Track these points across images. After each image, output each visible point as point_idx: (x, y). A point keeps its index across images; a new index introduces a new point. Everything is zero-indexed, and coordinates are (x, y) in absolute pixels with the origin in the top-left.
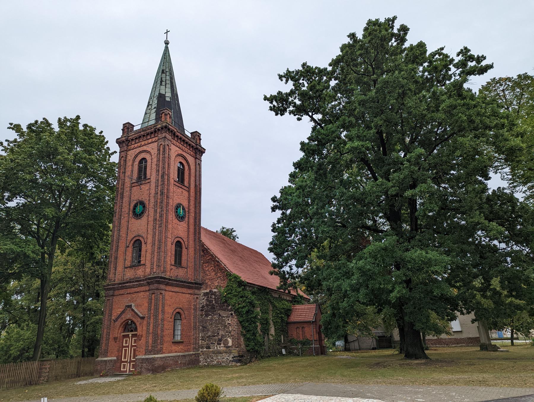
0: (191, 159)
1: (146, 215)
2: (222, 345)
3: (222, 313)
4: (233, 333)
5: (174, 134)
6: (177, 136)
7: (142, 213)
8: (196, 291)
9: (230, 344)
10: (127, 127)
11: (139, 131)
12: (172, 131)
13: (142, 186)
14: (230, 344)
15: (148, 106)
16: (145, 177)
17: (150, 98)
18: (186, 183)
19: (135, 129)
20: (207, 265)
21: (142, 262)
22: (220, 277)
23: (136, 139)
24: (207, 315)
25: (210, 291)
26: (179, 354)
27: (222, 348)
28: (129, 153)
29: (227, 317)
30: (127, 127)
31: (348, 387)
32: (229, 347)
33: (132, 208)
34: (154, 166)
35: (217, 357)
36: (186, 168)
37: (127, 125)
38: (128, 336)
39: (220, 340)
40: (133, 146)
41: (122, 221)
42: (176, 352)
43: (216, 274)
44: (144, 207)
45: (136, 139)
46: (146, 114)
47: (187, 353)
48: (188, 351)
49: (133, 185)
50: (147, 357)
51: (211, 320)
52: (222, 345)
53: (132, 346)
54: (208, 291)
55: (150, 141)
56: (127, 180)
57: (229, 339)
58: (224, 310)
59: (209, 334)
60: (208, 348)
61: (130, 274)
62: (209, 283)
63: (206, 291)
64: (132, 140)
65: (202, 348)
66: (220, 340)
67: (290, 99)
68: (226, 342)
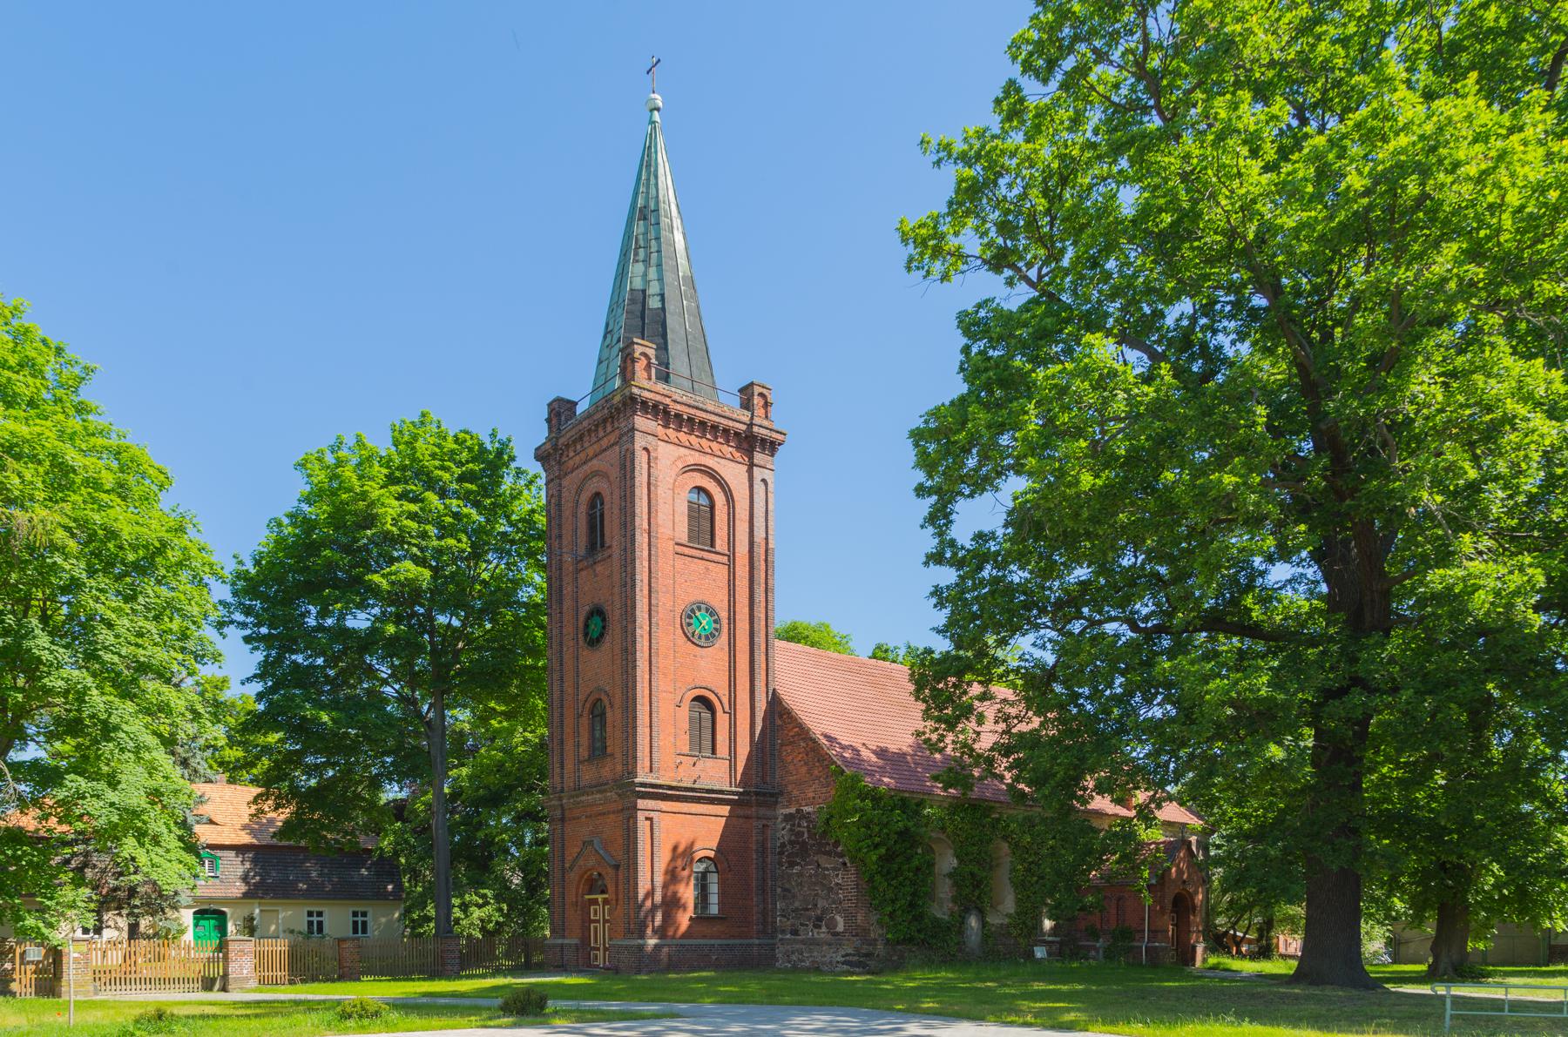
0: (734, 473)
1: (608, 638)
2: (824, 929)
3: (825, 861)
4: (846, 905)
5: (666, 412)
6: (678, 416)
7: (602, 635)
8: (769, 813)
9: (840, 928)
10: (560, 411)
11: (588, 415)
12: (655, 406)
13: (599, 568)
14: (840, 928)
15: (605, 337)
16: (602, 545)
17: (611, 310)
18: (721, 544)
19: (581, 409)
20: (789, 749)
21: (609, 750)
22: (818, 778)
23: (574, 442)
24: (792, 864)
25: (798, 811)
26: (731, 942)
27: (822, 933)
28: (565, 482)
29: (834, 869)
30: (560, 411)
31: (451, 1022)
32: (838, 934)
33: (581, 625)
34: (616, 511)
35: (811, 951)
36: (719, 499)
37: (555, 405)
38: (595, 902)
39: (820, 919)
40: (571, 463)
41: (566, 657)
42: (704, 937)
43: (809, 772)
44: (604, 620)
45: (574, 442)
46: (600, 362)
47: (737, 941)
48: (741, 937)
49: (580, 566)
50: (626, 942)
51: (800, 875)
52: (824, 929)
53: (605, 921)
54: (793, 810)
55: (605, 443)
56: (568, 558)
57: (838, 918)
58: (829, 853)
59: (797, 904)
60: (795, 932)
61: (588, 775)
62: (795, 793)
63: (787, 811)
64: (567, 446)
65: (783, 932)
66: (820, 919)
67: (1281, 108)
68: (831, 925)
